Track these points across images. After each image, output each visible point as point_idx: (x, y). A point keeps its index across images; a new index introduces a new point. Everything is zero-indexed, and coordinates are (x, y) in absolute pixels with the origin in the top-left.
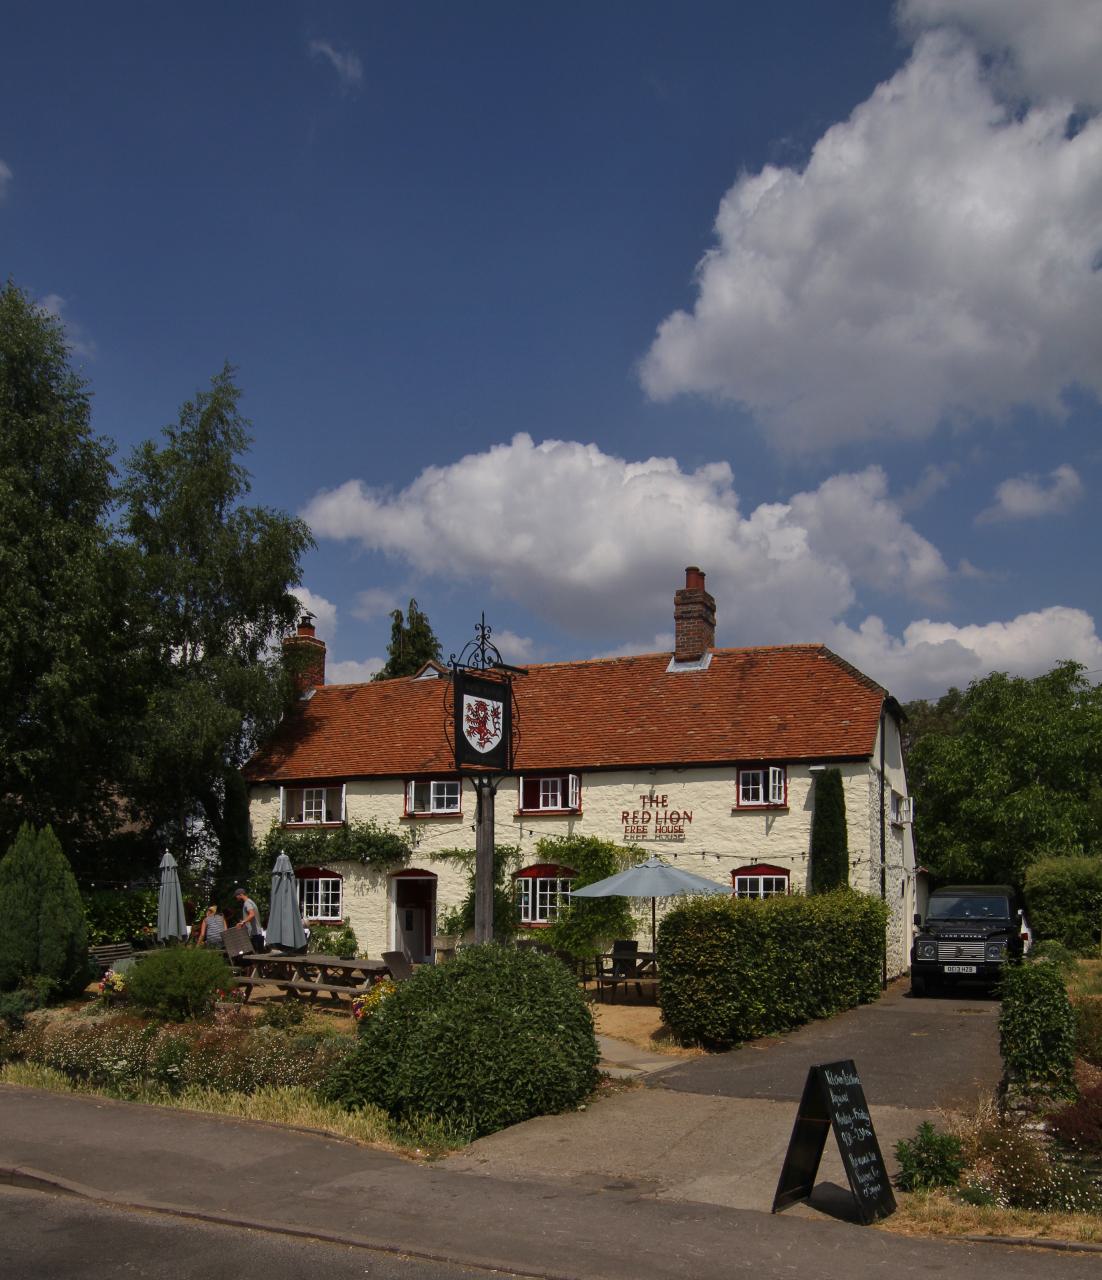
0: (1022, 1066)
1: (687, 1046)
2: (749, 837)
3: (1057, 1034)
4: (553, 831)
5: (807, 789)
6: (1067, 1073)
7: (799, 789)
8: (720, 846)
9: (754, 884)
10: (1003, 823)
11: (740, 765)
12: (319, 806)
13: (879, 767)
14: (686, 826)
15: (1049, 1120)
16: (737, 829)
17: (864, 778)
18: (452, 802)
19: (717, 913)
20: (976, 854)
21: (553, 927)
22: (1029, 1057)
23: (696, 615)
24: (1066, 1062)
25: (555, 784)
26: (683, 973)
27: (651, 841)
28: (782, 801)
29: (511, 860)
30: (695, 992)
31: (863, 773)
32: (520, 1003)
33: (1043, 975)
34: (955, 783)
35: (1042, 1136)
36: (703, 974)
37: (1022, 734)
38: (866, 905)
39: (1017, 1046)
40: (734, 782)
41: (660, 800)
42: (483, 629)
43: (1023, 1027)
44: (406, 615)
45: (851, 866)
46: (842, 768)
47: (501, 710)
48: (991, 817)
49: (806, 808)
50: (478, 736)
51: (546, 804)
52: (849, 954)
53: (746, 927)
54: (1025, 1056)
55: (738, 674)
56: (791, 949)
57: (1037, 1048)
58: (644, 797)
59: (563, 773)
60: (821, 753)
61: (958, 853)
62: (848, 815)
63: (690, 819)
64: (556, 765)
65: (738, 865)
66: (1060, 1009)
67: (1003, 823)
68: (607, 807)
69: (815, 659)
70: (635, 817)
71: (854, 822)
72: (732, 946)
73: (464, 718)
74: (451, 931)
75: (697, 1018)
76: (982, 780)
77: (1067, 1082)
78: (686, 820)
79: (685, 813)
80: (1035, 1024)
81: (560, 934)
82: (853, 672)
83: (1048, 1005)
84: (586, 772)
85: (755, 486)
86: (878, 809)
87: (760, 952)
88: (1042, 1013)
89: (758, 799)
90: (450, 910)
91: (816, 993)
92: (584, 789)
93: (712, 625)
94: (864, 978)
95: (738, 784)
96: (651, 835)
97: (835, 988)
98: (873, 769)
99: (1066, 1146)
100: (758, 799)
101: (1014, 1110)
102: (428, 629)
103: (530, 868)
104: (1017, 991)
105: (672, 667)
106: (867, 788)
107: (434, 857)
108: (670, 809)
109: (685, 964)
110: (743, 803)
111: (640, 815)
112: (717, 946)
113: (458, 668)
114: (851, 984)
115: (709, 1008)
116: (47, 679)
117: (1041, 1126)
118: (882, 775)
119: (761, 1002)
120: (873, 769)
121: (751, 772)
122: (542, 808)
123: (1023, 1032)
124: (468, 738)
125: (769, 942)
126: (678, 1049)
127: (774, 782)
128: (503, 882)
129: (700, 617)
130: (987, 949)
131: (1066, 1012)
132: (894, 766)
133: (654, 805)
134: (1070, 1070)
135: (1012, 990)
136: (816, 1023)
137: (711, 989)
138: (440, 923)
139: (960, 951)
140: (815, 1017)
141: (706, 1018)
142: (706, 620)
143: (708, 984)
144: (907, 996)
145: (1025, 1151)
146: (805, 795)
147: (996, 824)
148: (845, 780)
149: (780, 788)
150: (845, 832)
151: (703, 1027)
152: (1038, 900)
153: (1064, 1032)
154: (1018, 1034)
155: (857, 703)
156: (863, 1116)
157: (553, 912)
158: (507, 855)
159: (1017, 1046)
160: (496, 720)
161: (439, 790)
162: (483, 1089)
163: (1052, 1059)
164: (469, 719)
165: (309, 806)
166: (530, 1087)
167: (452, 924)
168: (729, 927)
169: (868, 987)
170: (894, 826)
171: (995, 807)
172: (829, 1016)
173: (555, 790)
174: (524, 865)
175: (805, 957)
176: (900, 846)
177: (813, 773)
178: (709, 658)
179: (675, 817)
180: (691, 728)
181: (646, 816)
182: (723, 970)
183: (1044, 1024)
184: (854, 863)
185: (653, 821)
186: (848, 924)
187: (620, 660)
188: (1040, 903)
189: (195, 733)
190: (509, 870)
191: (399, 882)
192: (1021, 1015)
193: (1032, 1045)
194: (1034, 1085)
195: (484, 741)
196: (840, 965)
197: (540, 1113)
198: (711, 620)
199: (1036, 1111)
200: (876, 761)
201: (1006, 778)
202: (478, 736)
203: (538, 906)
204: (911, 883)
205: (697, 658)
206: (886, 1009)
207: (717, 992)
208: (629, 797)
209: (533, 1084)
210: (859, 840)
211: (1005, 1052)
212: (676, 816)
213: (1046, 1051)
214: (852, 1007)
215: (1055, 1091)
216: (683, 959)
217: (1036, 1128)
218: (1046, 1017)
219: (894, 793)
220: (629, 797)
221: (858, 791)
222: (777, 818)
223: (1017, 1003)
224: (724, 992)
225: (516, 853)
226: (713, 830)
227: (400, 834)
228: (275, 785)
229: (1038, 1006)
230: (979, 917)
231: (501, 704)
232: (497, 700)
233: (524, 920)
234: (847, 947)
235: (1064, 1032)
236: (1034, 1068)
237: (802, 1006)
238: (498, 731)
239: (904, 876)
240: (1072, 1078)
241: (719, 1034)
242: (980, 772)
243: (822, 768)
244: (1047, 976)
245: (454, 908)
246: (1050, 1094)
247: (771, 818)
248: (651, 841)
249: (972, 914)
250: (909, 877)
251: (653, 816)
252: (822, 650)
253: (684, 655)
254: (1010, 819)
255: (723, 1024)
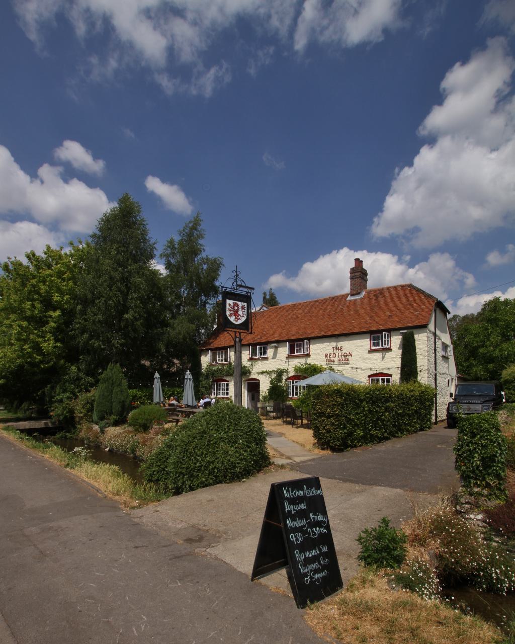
0: (468, 477)
1: (323, 449)
2: (375, 362)
3: (492, 458)
4: (299, 362)
5: (400, 341)
6: (499, 483)
7: (396, 341)
8: (363, 365)
9: (378, 380)
10: (498, 356)
11: (371, 332)
12: (222, 357)
13: (434, 331)
14: (350, 358)
15: (486, 513)
16: (370, 359)
17: (425, 334)
18: (265, 353)
19: (336, 390)
20: (487, 370)
21: (299, 399)
22: (473, 472)
23: (358, 276)
24: (498, 476)
25: (300, 344)
26: (321, 417)
27: (336, 365)
28: (389, 346)
29: (285, 374)
30: (326, 425)
31: (425, 332)
32: (222, 430)
33: (484, 420)
34: (477, 342)
35: (480, 523)
36: (329, 417)
37: (507, 320)
38: (423, 388)
39: (465, 465)
40: (369, 340)
41: (340, 348)
42: (236, 272)
43: (469, 453)
44: (268, 294)
45: (419, 373)
46: (415, 331)
47: (246, 306)
48: (492, 354)
49: (399, 348)
50: (235, 317)
51: (297, 352)
52: (414, 409)
53: (350, 396)
54: (470, 471)
55: (375, 298)
56: (379, 407)
57: (478, 467)
58: (333, 348)
59: (302, 340)
60: (405, 325)
61: (478, 370)
62: (417, 351)
63: (351, 355)
64: (301, 337)
65: (371, 373)
66: (495, 442)
67: (498, 356)
68: (319, 352)
69: (407, 289)
70: (330, 356)
71: (420, 353)
72: (343, 405)
73: (227, 309)
74: (264, 400)
75: (327, 437)
76: (488, 340)
77: (499, 489)
78: (350, 356)
79: (349, 353)
80: (477, 452)
81: (302, 401)
82: (423, 293)
83: (486, 439)
84: (311, 339)
85: (417, 258)
86: (434, 348)
87: (359, 408)
88: (482, 444)
89: (379, 346)
90: (264, 393)
91: (394, 426)
92: (311, 346)
93: (366, 281)
94: (422, 420)
95: (371, 340)
96: (336, 362)
97: (405, 424)
98: (430, 331)
99: (496, 532)
100: (379, 346)
101: (463, 504)
102: (276, 298)
103: (292, 377)
104: (466, 430)
105: (349, 298)
106: (426, 339)
107: (259, 373)
108: (343, 352)
109: (322, 413)
110: (373, 348)
111: (332, 355)
112: (335, 405)
113: (223, 289)
114: (415, 422)
115: (332, 432)
116: (126, 316)
117: (480, 517)
118: (435, 335)
119: (360, 430)
120: (430, 331)
121: (376, 335)
122: (296, 354)
123: (469, 456)
124: (229, 318)
125: (364, 403)
126: (320, 450)
127: (385, 338)
128: (282, 382)
129: (360, 277)
130: (482, 408)
131: (499, 444)
132: (443, 331)
133: (337, 350)
134: (501, 482)
135: (462, 430)
136: (395, 439)
137: (333, 424)
138: (261, 398)
139: (469, 409)
140: (395, 437)
141: (331, 437)
142: (362, 278)
143: (331, 422)
144: (445, 428)
145: (465, 535)
146: (399, 343)
147: (495, 357)
148: (416, 336)
149: (388, 341)
150: (416, 358)
151: (329, 441)
152: (508, 385)
153: (497, 457)
154: (466, 457)
155: (423, 304)
156: (320, 518)
157: (300, 393)
158: (283, 372)
159: (465, 465)
160: (243, 310)
161: (260, 349)
162: (194, 470)
163: (489, 474)
164: (229, 310)
165: (219, 357)
166: (216, 470)
167: (264, 398)
168: (341, 396)
169: (424, 424)
170: (443, 356)
171: (494, 350)
172: (401, 436)
173: (300, 347)
174: (290, 376)
175: (386, 410)
176: (447, 365)
177: (402, 333)
178: (364, 293)
179: (345, 355)
180: (353, 320)
181: (334, 355)
182: (337, 415)
183: (483, 452)
184: (420, 371)
185: (337, 357)
186: (412, 396)
187: (330, 298)
188: (509, 386)
189: (180, 333)
190: (284, 377)
191: (248, 383)
192: (467, 445)
193: (474, 464)
194: (476, 490)
195: (237, 319)
196: (408, 414)
197: (221, 482)
198: (365, 279)
199: (478, 506)
200: (431, 327)
201: (500, 338)
202: (235, 317)
203: (295, 391)
204: (454, 381)
205: (358, 294)
206: (433, 433)
207: (335, 425)
208: (328, 348)
209: (217, 468)
210: (423, 361)
211: (458, 468)
212: (345, 355)
213: (484, 469)
214: (415, 432)
215: (490, 495)
216: (321, 410)
217: (476, 517)
218: (484, 447)
219: (443, 343)
220: (328, 348)
221: (422, 341)
222: (387, 354)
223: (466, 437)
224: (339, 426)
225: (287, 371)
226: (361, 359)
227: (247, 365)
228: (207, 350)
229: (480, 440)
230: (480, 394)
231: (246, 304)
232: (244, 302)
233: (289, 396)
234: (412, 406)
235: (497, 457)
236: (476, 479)
237: (386, 432)
238: (244, 315)
239: (449, 378)
240: (502, 487)
241: (336, 445)
242: (488, 336)
243: (406, 331)
244: (487, 421)
245: (266, 392)
246: (487, 496)
247: (384, 353)
248: (336, 365)
249: (477, 392)
250: (452, 379)
251: (337, 354)
252: (410, 286)
253: (354, 292)
254: (501, 355)
255: (338, 440)
